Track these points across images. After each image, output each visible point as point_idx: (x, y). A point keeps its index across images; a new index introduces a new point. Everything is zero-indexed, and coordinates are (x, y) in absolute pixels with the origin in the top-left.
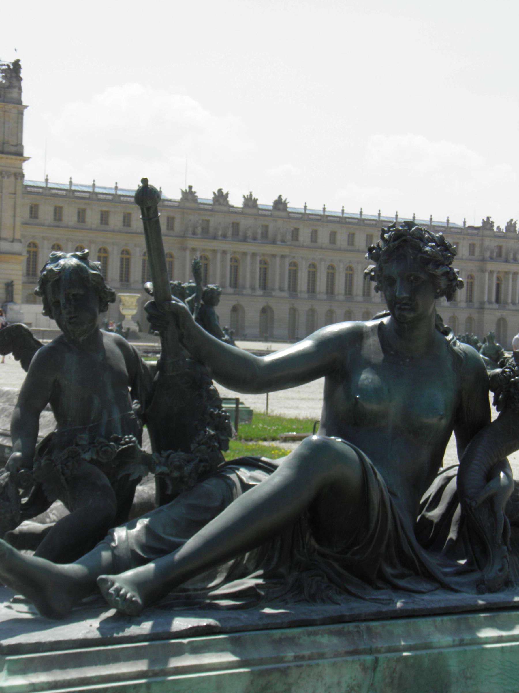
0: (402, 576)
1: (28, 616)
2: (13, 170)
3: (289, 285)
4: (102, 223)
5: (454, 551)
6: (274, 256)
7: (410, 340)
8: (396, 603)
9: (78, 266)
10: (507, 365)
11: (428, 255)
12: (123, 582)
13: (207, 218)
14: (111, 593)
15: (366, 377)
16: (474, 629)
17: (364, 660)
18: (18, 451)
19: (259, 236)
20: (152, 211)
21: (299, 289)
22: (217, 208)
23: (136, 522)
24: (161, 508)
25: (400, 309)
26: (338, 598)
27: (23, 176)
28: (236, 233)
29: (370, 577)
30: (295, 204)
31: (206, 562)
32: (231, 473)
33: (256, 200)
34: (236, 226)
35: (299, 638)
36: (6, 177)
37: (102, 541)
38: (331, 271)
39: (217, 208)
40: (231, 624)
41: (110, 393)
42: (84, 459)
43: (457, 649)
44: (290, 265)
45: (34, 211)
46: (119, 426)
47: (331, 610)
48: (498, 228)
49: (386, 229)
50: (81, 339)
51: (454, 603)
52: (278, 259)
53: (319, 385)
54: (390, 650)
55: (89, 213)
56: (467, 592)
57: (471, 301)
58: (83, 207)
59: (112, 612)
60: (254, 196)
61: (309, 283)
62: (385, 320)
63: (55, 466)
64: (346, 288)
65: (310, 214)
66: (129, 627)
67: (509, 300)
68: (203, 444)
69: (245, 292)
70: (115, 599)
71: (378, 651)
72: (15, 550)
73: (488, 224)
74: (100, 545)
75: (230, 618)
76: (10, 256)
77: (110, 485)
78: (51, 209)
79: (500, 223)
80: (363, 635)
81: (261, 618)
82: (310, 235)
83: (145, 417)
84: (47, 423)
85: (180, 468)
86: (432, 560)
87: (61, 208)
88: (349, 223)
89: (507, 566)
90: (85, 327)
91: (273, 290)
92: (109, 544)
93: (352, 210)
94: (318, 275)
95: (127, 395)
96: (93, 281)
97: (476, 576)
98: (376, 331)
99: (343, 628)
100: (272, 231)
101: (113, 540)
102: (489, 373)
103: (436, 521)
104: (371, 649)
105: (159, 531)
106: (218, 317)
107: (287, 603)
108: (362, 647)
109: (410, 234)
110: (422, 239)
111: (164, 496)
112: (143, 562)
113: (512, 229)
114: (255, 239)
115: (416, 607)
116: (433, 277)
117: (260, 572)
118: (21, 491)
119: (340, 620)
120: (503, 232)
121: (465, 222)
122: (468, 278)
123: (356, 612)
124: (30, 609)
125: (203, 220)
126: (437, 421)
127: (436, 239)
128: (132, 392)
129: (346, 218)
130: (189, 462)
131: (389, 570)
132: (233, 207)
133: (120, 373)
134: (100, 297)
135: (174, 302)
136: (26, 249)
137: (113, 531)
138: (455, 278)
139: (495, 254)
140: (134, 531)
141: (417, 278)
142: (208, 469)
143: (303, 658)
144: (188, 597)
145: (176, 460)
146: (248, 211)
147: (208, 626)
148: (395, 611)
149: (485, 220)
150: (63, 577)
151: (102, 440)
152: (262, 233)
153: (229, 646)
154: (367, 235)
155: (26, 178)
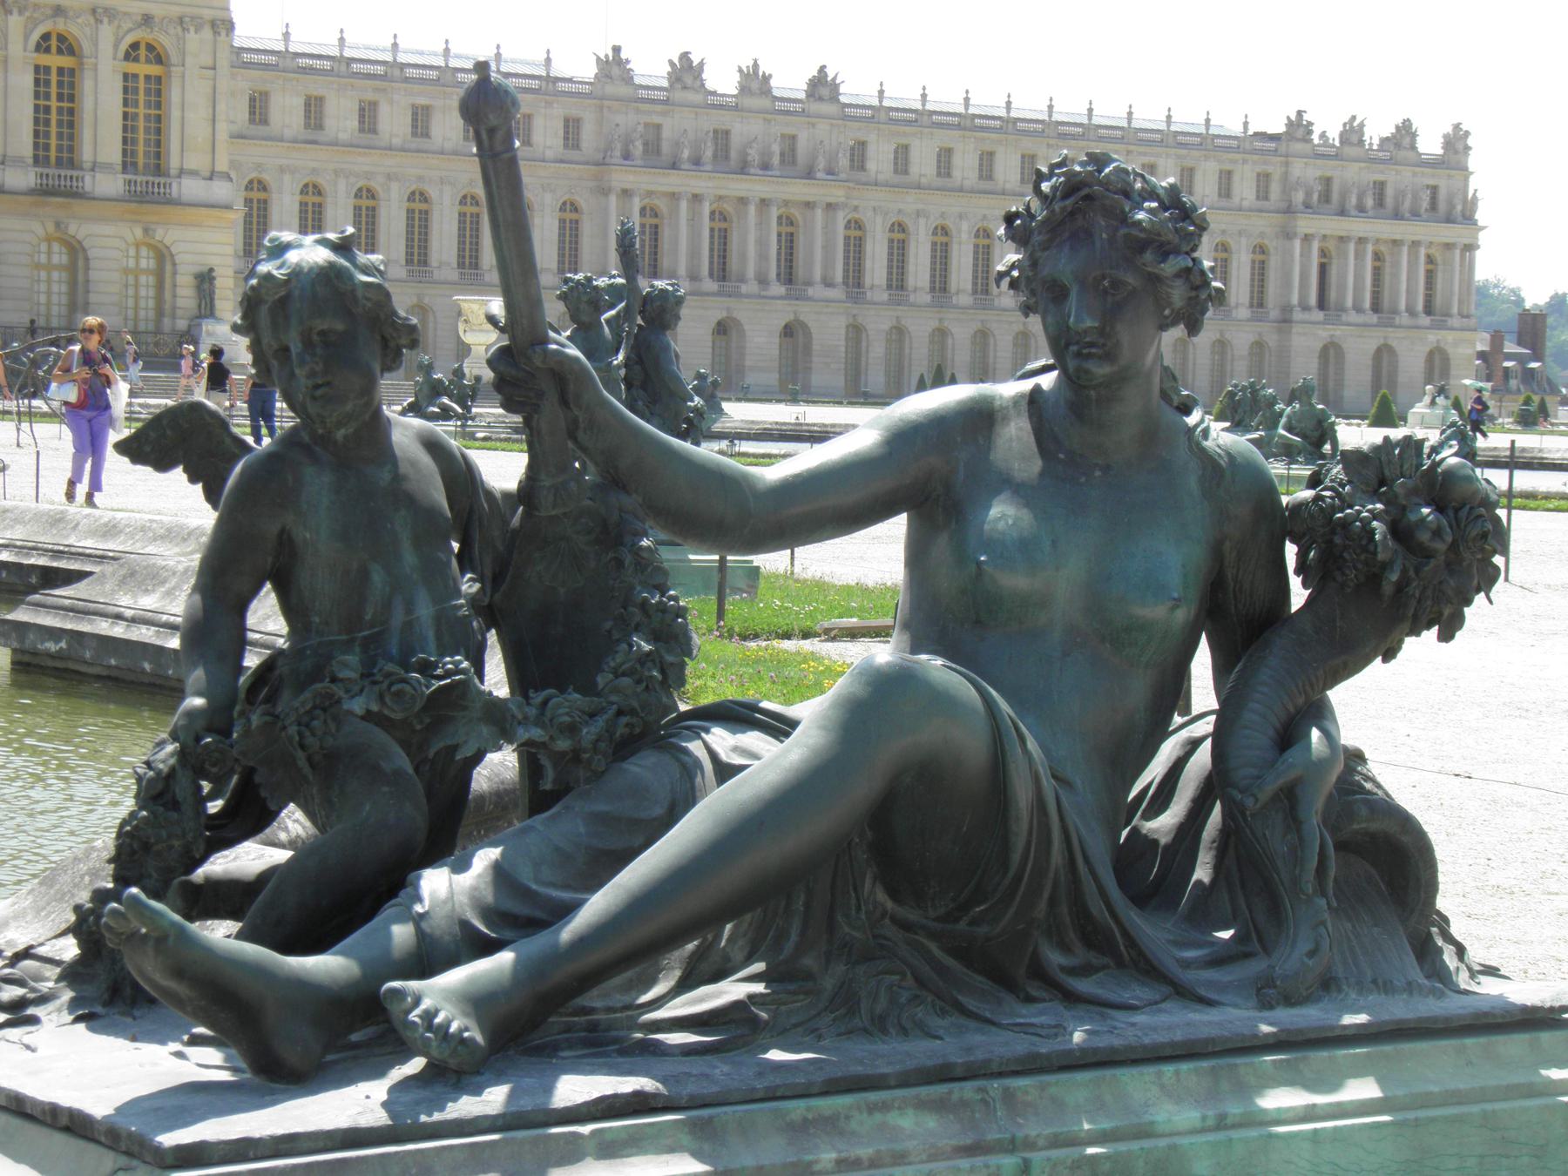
0: (1085, 971)
1: (225, 1076)
2: (208, 14)
3: (846, 271)
4: (414, 134)
5: (1205, 910)
6: (809, 205)
7: (1097, 430)
8: (1071, 1034)
9: (332, 265)
10: (1327, 482)
11: (1143, 230)
12: (441, 996)
13: (656, 119)
14: (414, 1023)
15: (1002, 514)
16: (1247, 1091)
17: (999, 1167)
18: (199, 694)
19: (776, 160)
20: (499, 136)
22: (679, 95)
23: (472, 856)
24: (529, 822)
25: (1078, 355)
26: (936, 1022)
27: (230, 26)
28: (723, 153)
29: (1010, 973)
30: (856, 88)
31: (634, 946)
32: (690, 740)
33: (766, 79)
34: (722, 137)
35: (848, 1118)
36: (192, 29)
37: (393, 902)
38: (941, 239)
39: (679, 95)
40: (690, 1088)
41: (409, 558)
42: (350, 713)
43: (1211, 1137)
44: (847, 227)
45: (258, 108)
46: (431, 635)
47: (919, 1051)
48: (1323, 135)
49: (1045, 170)
50: (340, 434)
51: (1205, 1033)
52: (819, 212)
53: (896, 528)
54: (1056, 1142)
55: (384, 111)
56: (1236, 1006)
57: (1261, 305)
58: (370, 96)
59: (416, 1065)
60: (764, 68)
61: (890, 267)
62: (1047, 381)
63: (284, 728)
64: (975, 277)
65: (891, 109)
66: (455, 1100)
67: (1349, 303)
68: (624, 674)
69: (744, 289)
70: (422, 1036)
71: (1030, 1145)
72: (187, 924)
73: (1299, 128)
74: (388, 911)
75: (689, 1075)
76: (204, 211)
77: (410, 771)
78: (299, 102)
79: (1327, 126)
80: (995, 1110)
81: (760, 1074)
82: (892, 156)
83: (489, 612)
84: (267, 619)
85: (572, 730)
86: (1154, 932)
87: (320, 100)
88: (983, 129)
89: (1326, 944)
90: (349, 407)
91: (809, 283)
92: (410, 908)
93: (988, 101)
95: (449, 562)
96: (368, 299)
97: (1256, 967)
98: (1024, 403)
99: (950, 1093)
100: (808, 142)
101: (419, 899)
102: (1285, 500)
103: (1164, 840)
104: (1013, 1140)
105: (526, 876)
106: (677, 356)
107: (820, 1037)
108: (993, 1136)
109: (1100, 183)
110: (1127, 193)
111: (540, 791)
112: (487, 947)
113: (1354, 139)
114: (765, 166)
115: (1117, 1042)
116: (1154, 280)
117: (759, 967)
118: (206, 786)
119: (943, 1074)
120: (1333, 146)
121: (1246, 124)
122: (1254, 252)
123: (980, 1055)
124: (226, 1060)
125: (646, 125)
126: (1167, 612)
127: (1161, 192)
128: (460, 556)
129: (975, 116)
130: (592, 715)
131: (1054, 958)
132: (714, 93)
133: (431, 513)
134: (383, 337)
135: (554, 347)
136: (243, 194)
137: (419, 878)
138: (1206, 284)
139: (1315, 197)
140: (467, 879)
141: (1116, 284)
142: (637, 730)
144: (593, 1027)
145: (561, 711)
146: (749, 102)
147: (638, 1095)
148: (1070, 1052)
149: (1293, 118)
150: (302, 986)
151: (390, 667)
152: (782, 154)
153: (685, 1139)
154: (1023, 157)
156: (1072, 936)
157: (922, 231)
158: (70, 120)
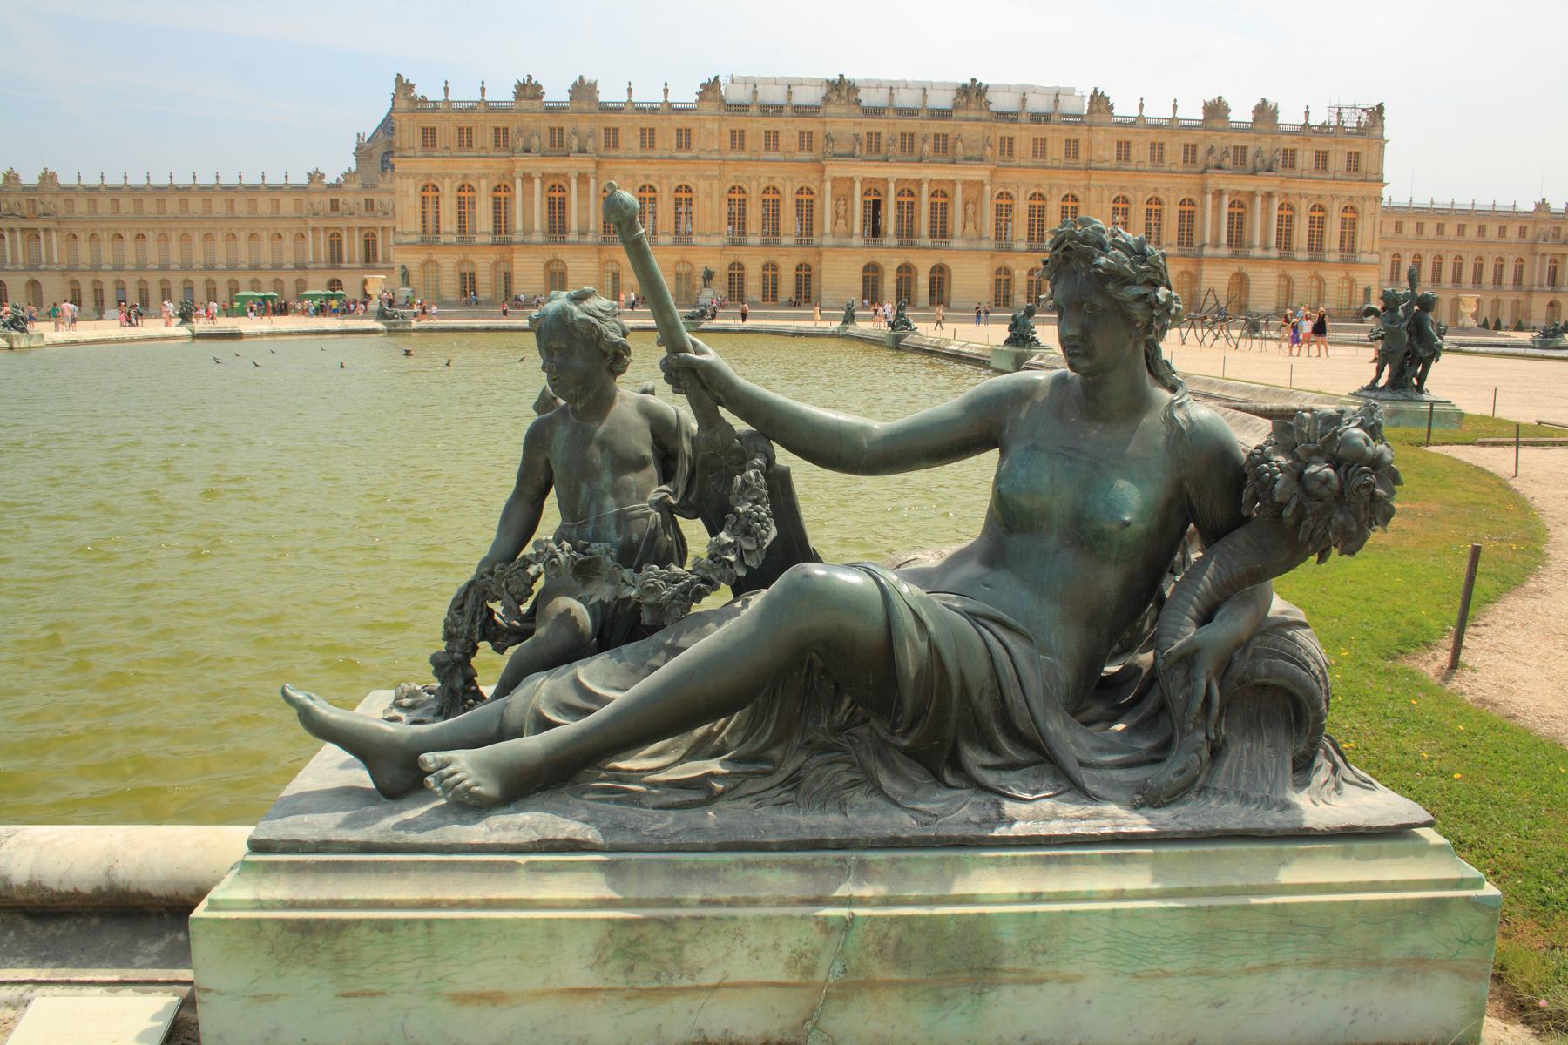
21: (1326, 247)
29: (939, 761)
91: (1251, 247)
94: (1328, 222)
143: (717, 903)
155: (1116, 112)
156: (1004, 743)
157: (665, 190)
158: (1321, 235)
